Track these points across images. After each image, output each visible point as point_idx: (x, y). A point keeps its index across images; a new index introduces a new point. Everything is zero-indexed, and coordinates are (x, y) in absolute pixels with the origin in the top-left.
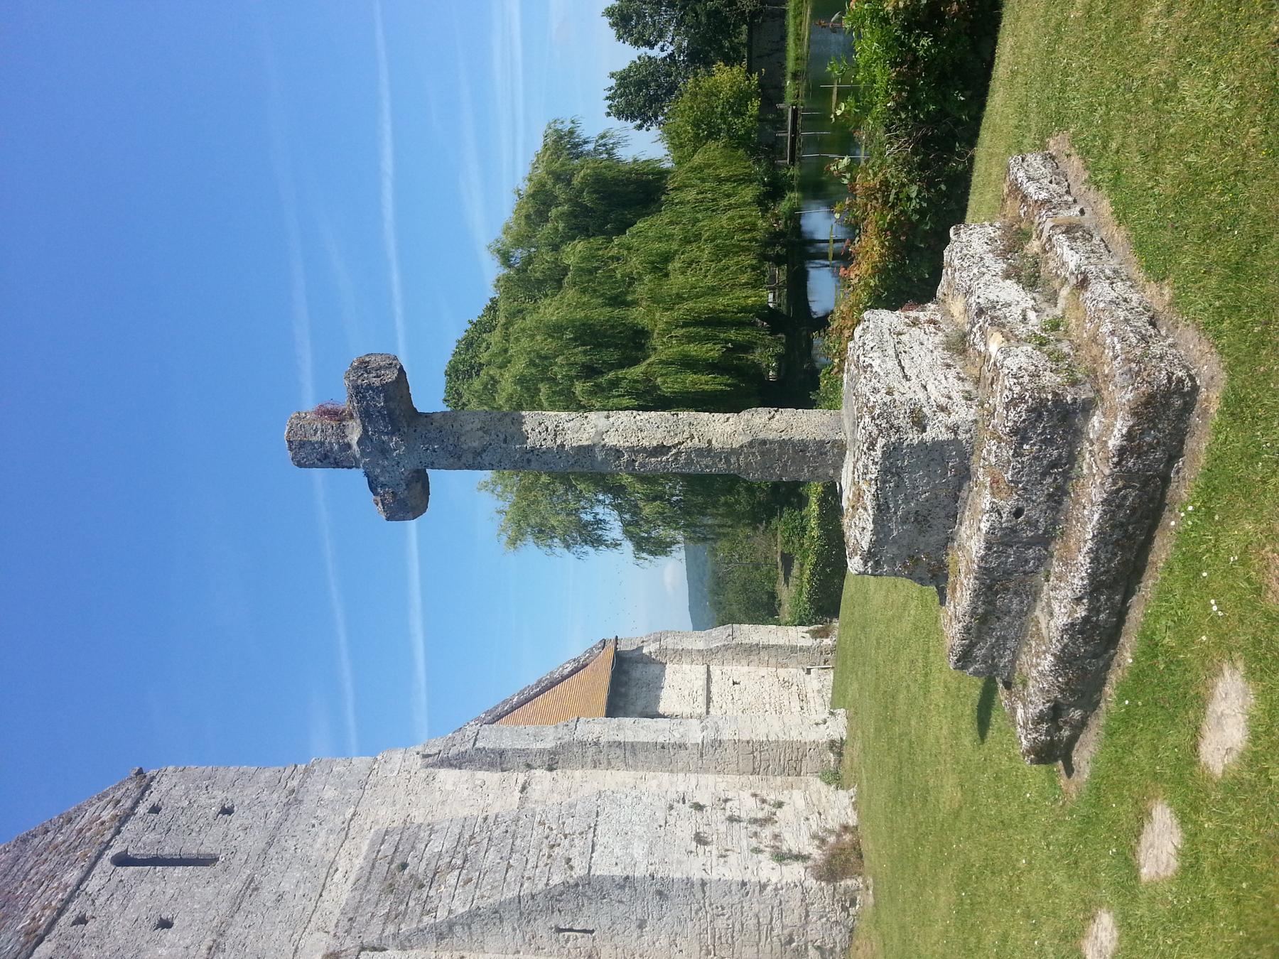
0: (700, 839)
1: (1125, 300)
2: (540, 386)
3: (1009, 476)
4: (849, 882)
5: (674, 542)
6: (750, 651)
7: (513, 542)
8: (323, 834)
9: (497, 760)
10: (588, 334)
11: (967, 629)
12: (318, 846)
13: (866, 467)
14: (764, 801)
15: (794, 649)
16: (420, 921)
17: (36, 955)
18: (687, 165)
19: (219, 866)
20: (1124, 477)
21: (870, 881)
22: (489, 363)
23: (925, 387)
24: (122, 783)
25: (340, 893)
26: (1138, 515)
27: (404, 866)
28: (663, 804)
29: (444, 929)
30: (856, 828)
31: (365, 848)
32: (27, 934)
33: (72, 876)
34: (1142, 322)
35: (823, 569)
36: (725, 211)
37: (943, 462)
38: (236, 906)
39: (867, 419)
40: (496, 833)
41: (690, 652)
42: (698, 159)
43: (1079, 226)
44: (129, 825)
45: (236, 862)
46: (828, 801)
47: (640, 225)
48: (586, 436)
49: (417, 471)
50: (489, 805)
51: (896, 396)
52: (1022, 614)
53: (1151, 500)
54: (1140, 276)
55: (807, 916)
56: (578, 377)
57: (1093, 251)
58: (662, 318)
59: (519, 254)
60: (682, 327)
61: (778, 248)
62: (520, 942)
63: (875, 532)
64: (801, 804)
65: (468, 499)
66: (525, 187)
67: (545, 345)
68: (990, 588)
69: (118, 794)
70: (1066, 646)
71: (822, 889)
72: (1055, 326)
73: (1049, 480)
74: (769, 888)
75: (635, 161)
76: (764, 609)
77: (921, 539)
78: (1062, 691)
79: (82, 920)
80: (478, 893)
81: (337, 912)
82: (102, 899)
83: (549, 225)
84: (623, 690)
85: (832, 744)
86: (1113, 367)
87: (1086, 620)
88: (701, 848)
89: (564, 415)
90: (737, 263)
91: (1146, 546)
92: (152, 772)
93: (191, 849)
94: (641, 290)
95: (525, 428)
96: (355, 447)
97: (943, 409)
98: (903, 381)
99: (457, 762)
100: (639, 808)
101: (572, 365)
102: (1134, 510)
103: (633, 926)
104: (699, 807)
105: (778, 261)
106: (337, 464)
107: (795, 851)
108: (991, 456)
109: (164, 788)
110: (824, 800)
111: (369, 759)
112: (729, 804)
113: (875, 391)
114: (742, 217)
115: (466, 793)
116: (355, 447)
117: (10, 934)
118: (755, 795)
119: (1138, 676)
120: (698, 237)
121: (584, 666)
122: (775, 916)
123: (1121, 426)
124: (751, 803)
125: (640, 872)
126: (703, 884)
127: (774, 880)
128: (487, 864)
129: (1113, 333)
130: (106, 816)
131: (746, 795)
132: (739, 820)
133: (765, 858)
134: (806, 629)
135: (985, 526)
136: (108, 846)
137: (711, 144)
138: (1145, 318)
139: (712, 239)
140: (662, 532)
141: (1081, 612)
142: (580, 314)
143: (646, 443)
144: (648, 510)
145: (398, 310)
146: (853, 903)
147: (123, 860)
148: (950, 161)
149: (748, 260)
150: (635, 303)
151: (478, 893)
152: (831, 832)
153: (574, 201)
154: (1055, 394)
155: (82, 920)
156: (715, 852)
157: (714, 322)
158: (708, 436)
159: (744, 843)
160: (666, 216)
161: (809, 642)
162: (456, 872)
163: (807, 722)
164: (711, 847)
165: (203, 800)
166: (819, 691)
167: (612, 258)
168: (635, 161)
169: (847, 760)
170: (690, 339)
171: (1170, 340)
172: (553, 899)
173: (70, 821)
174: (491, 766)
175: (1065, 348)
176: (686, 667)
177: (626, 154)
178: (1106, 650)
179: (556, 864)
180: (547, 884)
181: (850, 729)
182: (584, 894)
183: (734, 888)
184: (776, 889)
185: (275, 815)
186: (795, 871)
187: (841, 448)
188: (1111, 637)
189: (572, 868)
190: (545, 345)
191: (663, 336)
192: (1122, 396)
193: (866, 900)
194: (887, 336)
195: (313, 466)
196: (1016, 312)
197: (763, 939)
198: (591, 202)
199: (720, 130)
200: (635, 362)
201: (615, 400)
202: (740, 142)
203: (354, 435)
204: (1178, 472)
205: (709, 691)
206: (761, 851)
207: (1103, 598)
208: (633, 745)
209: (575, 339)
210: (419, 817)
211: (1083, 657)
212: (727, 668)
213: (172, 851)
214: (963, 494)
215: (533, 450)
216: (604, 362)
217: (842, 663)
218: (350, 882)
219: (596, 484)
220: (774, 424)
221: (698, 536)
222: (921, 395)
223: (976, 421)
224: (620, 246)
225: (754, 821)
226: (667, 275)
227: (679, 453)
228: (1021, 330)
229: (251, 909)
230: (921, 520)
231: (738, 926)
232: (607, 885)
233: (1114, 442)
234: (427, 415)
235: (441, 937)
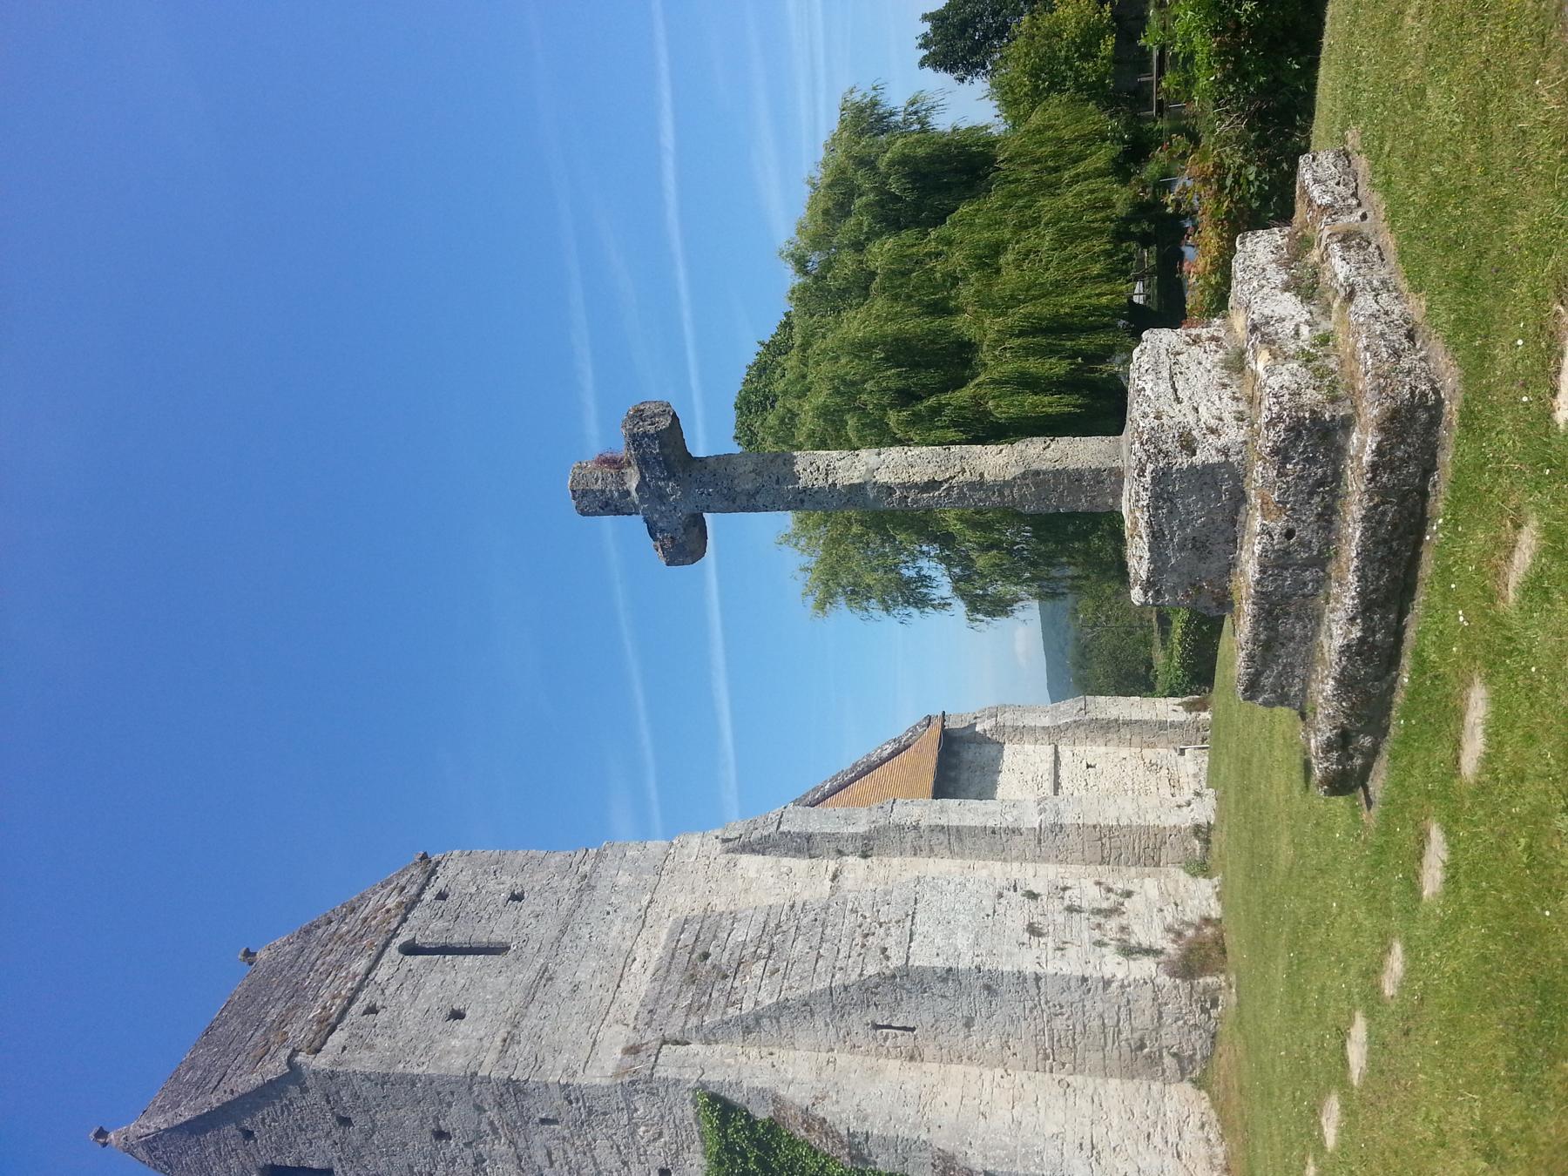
0: (1033, 930)
1: (1386, 313)
2: (847, 417)
3: (1275, 497)
4: (1209, 980)
5: (1017, 599)
6: (1108, 728)
7: (822, 605)
8: (618, 922)
9: (804, 845)
10: (902, 352)
11: (1251, 657)
12: (614, 934)
13: (1137, 493)
14: (1109, 890)
15: (1162, 725)
16: (725, 1013)
17: (329, 1043)
18: (1022, 129)
19: (510, 955)
20: (1379, 493)
21: (1233, 978)
22: (785, 393)
23: (1196, 410)
24: (406, 869)
25: (639, 984)
26: (1401, 529)
27: (706, 956)
28: (991, 892)
29: (751, 1023)
30: (1220, 920)
31: (663, 936)
32: (320, 1022)
33: (360, 965)
34: (1397, 337)
35: (1198, 627)
36: (1069, 185)
37: (1216, 486)
38: (530, 998)
39: (1137, 445)
40: (805, 921)
41: (1033, 729)
42: (1036, 119)
43: (1358, 233)
44: (415, 913)
45: (528, 950)
46: (1187, 891)
47: (964, 209)
48: (857, 474)
49: (694, 515)
50: (796, 894)
51: (1165, 419)
52: (1306, 639)
53: (1412, 514)
54: (1404, 286)
55: (1160, 1017)
56: (892, 406)
57: (1365, 261)
58: (993, 325)
59: (816, 258)
60: (1018, 336)
61: (1145, 225)
62: (834, 1039)
63: (1152, 560)
65: (759, 548)
66: (819, 175)
67: (847, 367)
68: (1270, 613)
69: (403, 881)
70: (1345, 668)
71: (1176, 987)
72: (1325, 340)
73: (1317, 499)
74: (1114, 985)
75: (955, 130)
76: (1138, 682)
77: (1202, 566)
78: (1347, 716)
79: (372, 1010)
80: (786, 984)
81: (637, 1004)
82: (392, 989)
83: (852, 221)
84: (953, 774)
85: (1197, 830)
86: (1365, 384)
87: (1362, 640)
88: (1035, 940)
89: (835, 453)
90: (1088, 250)
91: (1414, 562)
92: (435, 857)
93: (481, 937)
94: (966, 292)
95: (796, 468)
96: (634, 493)
97: (1213, 431)
98: (1174, 404)
99: (760, 847)
100: (964, 895)
101: (885, 390)
102: (1395, 526)
103: (959, 1025)
104: (1033, 896)
105: (1145, 240)
106: (617, 511)
107: (1145, 944)
108: (1259, 474)
109: (450, 873)
110: (1182, 889)
111: (665, 843)
112: (1068, 893)
113: (1145, 415)
114: (1092, 192)
115: (771, 881)
116: (634, 493)
117: (301, 1024)
118: (1099, 883)
119: (1413, 695)
120: (1036, 221)
121: (906, 747)
122: (1122, 1017)
123: (1371, 442)
125: (964, 964)
126: (1038, 978)
127: (1120, 976)
128: (795, 953)
129: (1367, 348)
130: (391, 903)
131: (1088, 884)
132: (1079, 910)
134: (1178, 700)
135: (1257, 549)
136: (395, 934)
137: (1055, 98)
138: (1402, 331)
139: (1053, 223)
140: (1000, 588)
141: (1356, 633)
142: (890, 328)
143: (917, 479)
144: (982, 562)
145: (686, 314)
146: (1215, 1004)
147: (410, 949)
148: (1292, 135)
149: (1100, 245)
150: (959, 310)
151: (786, 984)
152: (1189, 924)
153: (881, 190)
154: (1313, 412)
155: (372, 1010)
156: (1051, 945)
157: (1058, 328)
158: (980, 469)
159: (1085, 935)
160: (995, 200)
161: (1182, 716)
162: (762, 962)
164: (1049, 940)
165: (492, 885)
166: (1195, 776)
167: (929, 255)
168: (955, 130)
169: (1215, 848)
170: (1029, 352)
171: (1423, 353)
172: (869, 991)
173: (353, 910)
174: (798, 852)
175: (1332, 364)
176: (1028, 747)
177: (942, 123)
178: (1388, 672)
179: (871, 953)
180: (861, 975)
181: (1220, 811)
182: (902, 987)
183: (1073, 983)
184: (1122, 986)
185: (568, 902)
187: (1118, 475)
188: (1391, 659)
189: (888, 958)
190: (847, 367)
191: (994, 348)
192: (1371, 412)
193: (1228, 999)
194: (1163, 357)
195: (595, 514)
196: (1289, 327)
197: (1110, 1042)
198: (907, 186)
199: (1064, 79)
200: (960, 384)
201: (938, 433)
202: (1095, 92)
203: (633, 483)
204: (1434, 486)
205: (1057, 776)
206: (1105, 945)
207: (1376, 617)
208: (958, 829)
209: (886, 359)
210: (720, 904)
211: (1364, 680)
212: (1079, 749)
213: (462, 939)
214: (1241, 518)
215: (805, 489)
216: (924, 386)
217: (1212, 740)
219: (919, 533)
220: (1049, 454)
221: (1048, 595)
222: (1191, 418)
223: (1245, 442)
224: (939, 240)
225: (1099, 912)
226: (998, 271)
227: (951, 488)
228: (1291, 347)
229: (546, 999)
230: (1199, 546)
231: (1079, 1028)
232: (928, 977)
233: (1367, 458)
234: (701, 460)
235: (747, 1030)
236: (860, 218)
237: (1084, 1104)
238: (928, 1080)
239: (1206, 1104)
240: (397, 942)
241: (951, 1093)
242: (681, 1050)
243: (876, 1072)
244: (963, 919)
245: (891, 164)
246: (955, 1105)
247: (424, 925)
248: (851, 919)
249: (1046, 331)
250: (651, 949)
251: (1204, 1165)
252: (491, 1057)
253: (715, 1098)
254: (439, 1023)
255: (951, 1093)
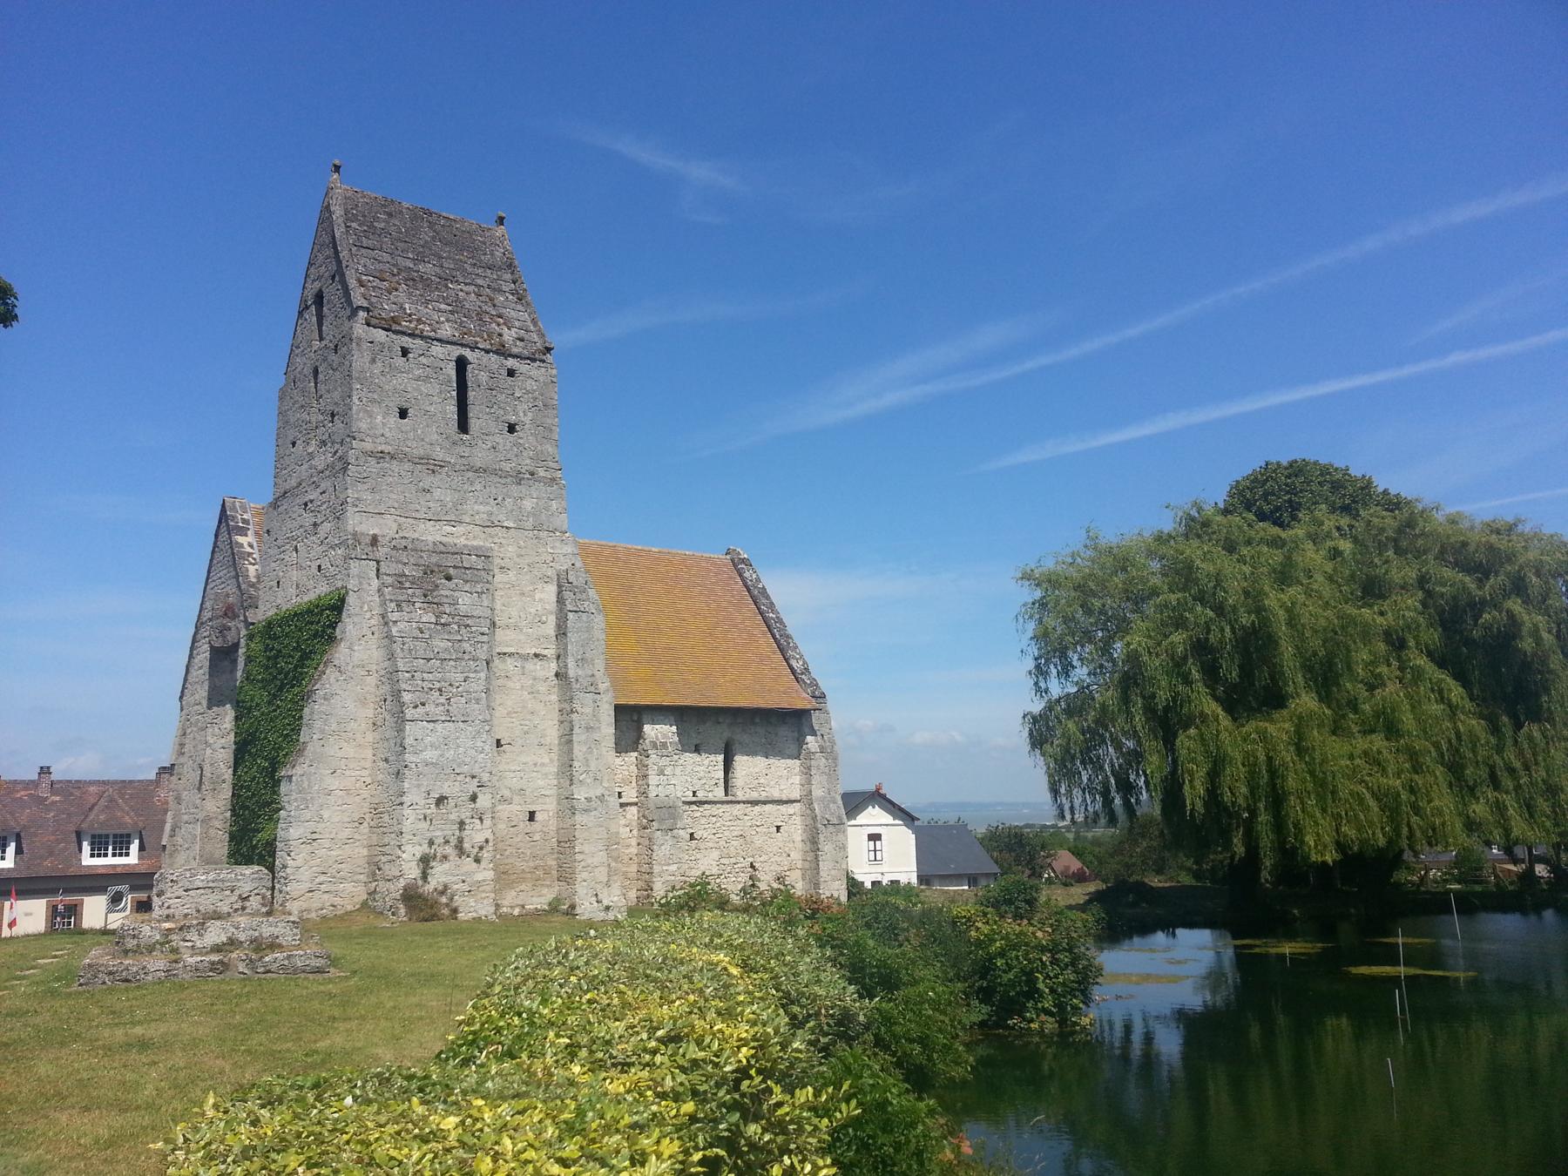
0: (441, 800)
4: (402, 911)
8: (488, 508)
14: (481, 848)
25: (431, 534)
27: (449, 578)
28: (476, 771)
41: (810, 783)
64: (479, 877)
81: (416, 535)
85: (573, 907)
88: (433, 801)
93: (473, 412)
104: (474, 798)
109: (534, 373)
118: (487, 841)
124: (479, 838)
133: (425, 848)
142: (1282, 630)
147: (461, 364)
155: (405, 352)
159: (438, 833)
163: (599, 887)
170: (1252, 775)
174: (559, 626)
185: (507, 466)
186: (413, 872)
205: (765, 803)
212: (798, 820)
218: (444, 540)
225: (461, 840)
236: (1450, 579)
237: (347, 833)
238: (358, 736)
239: (349, 908)
240: (467, 353)
241: (349, 750)
242: (373, 574)
243: (363, 702)
244: (450, 754)
245: (1511, 615)
246: (340, 754)
247: (483, 366)
248: (460, 677)
249: (1272, 784)
250: (460, 536)
251: (305, 906)
252: (368, 446)
253: (342, 600)
254: (394, 404)
255: (349, 750)
